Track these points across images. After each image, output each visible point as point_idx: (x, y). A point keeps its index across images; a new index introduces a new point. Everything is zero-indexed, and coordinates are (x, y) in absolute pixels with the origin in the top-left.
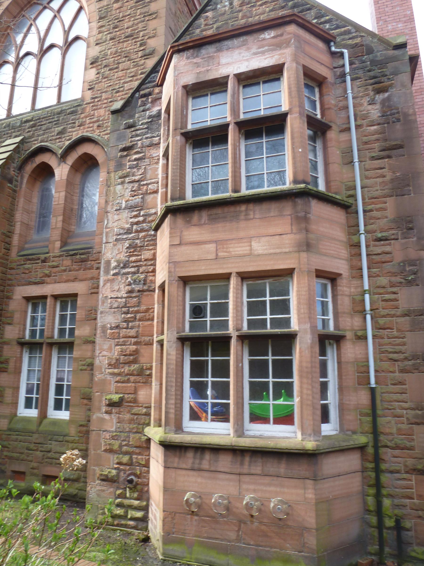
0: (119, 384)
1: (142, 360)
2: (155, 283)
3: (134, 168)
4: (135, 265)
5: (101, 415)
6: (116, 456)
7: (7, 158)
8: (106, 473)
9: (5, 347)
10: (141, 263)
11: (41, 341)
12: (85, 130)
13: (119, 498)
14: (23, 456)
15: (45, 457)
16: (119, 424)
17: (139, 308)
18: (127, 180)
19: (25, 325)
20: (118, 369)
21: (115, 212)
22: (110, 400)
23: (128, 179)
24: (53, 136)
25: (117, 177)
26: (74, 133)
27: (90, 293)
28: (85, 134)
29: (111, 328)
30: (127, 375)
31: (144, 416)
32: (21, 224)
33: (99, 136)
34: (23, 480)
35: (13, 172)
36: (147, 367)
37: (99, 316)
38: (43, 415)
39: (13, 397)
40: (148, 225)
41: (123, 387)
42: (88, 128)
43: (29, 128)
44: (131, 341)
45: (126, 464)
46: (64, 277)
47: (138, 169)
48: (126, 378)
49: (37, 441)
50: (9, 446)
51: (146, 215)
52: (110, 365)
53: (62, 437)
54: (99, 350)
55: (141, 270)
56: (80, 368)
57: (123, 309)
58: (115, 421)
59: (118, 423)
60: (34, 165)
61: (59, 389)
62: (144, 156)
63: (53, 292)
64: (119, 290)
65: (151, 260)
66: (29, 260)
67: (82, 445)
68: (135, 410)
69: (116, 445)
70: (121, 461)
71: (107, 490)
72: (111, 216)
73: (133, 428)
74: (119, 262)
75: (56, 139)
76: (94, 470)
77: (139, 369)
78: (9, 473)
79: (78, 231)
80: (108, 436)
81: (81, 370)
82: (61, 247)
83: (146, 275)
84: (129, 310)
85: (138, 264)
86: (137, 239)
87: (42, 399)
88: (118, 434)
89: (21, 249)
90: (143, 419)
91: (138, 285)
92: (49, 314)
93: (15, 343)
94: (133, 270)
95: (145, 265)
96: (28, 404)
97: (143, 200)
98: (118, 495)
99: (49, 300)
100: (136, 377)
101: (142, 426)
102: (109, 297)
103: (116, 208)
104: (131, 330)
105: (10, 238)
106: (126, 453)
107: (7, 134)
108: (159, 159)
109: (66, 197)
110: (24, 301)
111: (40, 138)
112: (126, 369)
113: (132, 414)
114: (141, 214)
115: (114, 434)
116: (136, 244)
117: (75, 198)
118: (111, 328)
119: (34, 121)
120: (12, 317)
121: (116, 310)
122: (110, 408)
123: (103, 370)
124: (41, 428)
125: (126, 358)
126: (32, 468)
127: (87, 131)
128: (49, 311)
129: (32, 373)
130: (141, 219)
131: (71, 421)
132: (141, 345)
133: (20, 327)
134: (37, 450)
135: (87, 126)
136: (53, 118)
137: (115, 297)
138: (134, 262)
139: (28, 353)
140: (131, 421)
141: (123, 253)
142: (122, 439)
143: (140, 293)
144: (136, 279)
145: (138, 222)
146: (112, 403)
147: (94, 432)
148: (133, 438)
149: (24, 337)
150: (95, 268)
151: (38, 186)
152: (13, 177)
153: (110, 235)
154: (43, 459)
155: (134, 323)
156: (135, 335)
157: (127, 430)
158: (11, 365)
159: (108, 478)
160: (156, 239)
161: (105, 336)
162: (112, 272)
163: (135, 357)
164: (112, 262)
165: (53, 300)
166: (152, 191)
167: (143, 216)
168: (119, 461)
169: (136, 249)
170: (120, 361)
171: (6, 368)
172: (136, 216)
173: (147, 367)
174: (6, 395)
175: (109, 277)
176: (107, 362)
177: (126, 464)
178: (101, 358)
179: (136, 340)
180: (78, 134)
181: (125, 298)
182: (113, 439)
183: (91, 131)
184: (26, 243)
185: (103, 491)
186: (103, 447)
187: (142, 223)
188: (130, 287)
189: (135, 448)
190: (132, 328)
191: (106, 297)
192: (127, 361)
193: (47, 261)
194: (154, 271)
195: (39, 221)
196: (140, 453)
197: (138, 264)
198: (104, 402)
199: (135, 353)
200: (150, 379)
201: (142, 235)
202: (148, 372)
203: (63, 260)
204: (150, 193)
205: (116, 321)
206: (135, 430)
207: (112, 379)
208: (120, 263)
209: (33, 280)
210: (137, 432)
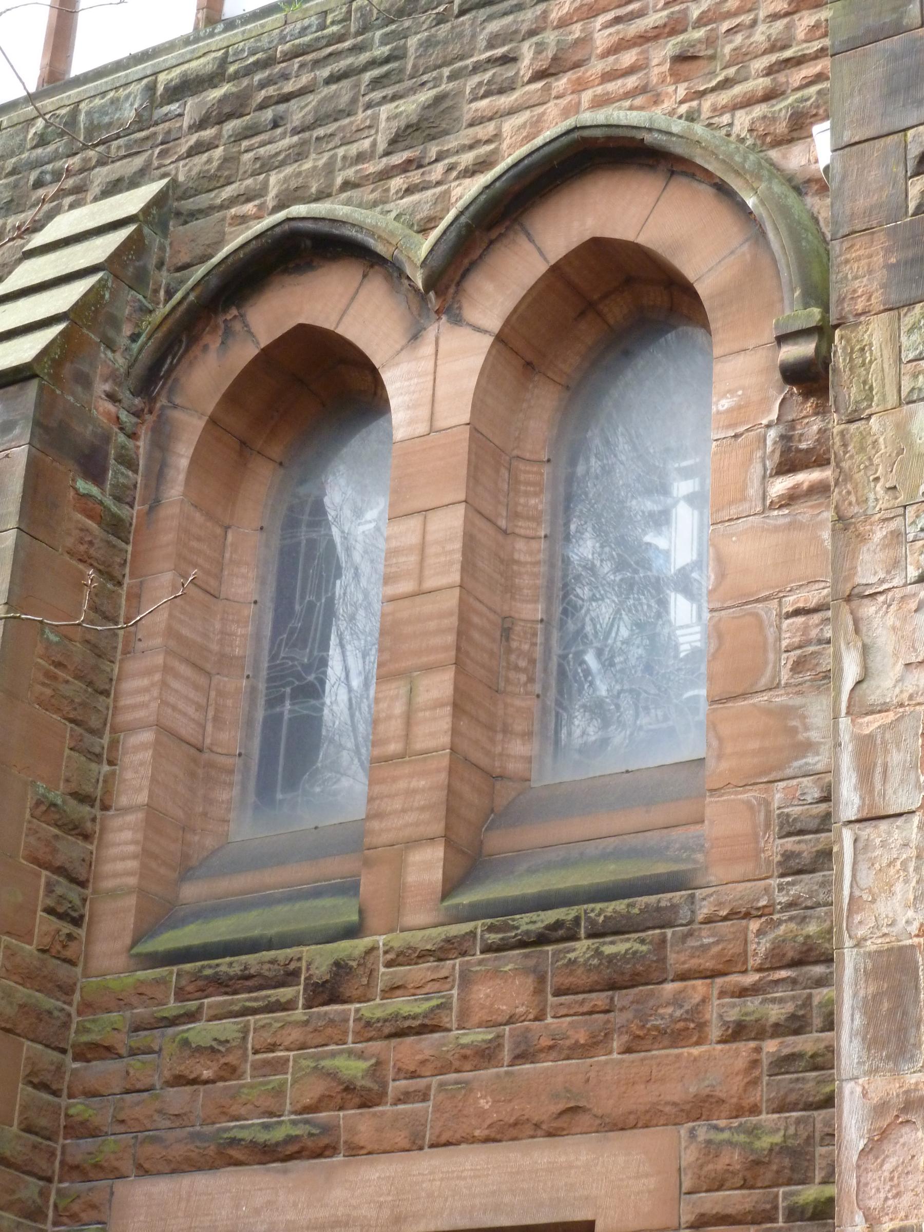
12: (586, 97)
24: (361, 158)
26: (508, 126)
27: (687, 1217)
28: (587, 117)
33: (691, 117)
35: (110, 407)
42: (608, 76)
43: (201, 125)
46: (485, 1104)
66: (222, 984)
72: (891, 620)
75: (386, 175)
82: (450, 888)
107: (57, 176)
109: (470, 543)
117: (521, 550)
119: (236, 76)
127: (599, 103)
135: (597, 67)
136: (357, 49)
150: (715, 1032)
152: (107, 438)
153: (896, 758)
180: (537, 125)
183: (628, 95)
193: (349, 989)
195: (272, 724)
203: (466, 980)
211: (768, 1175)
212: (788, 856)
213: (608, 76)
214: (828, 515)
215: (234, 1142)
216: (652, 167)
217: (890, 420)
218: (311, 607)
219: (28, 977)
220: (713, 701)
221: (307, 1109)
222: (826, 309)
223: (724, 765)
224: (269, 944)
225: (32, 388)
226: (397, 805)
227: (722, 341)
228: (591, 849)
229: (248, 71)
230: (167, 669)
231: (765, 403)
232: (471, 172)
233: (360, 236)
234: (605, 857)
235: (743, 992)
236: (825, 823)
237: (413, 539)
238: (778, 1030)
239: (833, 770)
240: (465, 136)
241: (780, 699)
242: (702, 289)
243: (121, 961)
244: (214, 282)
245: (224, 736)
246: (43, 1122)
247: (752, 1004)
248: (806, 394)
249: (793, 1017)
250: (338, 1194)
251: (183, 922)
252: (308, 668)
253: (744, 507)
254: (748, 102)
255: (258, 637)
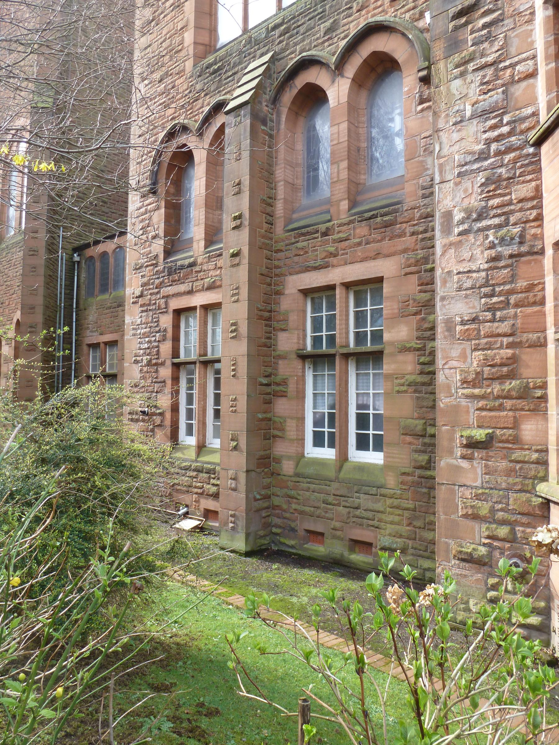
0: (484, 413)
1: (526, 372)
2: (542, 238)
3: (482, 42)
4: (499, 211)
5: (454, 462)
6: (484, 526)
7: (257, 87)
8: (469, 551)
9: (280, 362)
10: (512, 207)
11: (332, 351)
12: (370, 15)
13: (493, 590)
14: (318, 512)
15: (351, 515)
16: (487, 476)
17: (513, 285)
18: (471, 66)
19: (304, 330)
20: (479, 388)
21: (454, 128)
22: (469, 438)
23: (472, 64)
24: (318, 39)
25: (450, 66)
26: (352, 25)
27: (403, 273)
28: (370, 20)
29: (463, 323)
30: (499, 397)
31: (535, 466)
32: (285, 185)
33: (395, 16)
34: (322, 543)
35: (266, 108)
36: (535, 383)
37: (438, 304)
38: (343, 457)
39: (297, 430)
40: (521, 137)
41: (490, 417)
42: (375, 9)
43: (280, 36)
44: (502, 342)
45: (503, 540)
46: (360, 254)
47: (492, 43)
48: (497, 404)
49: (338, 493)
50: (299, 497)
51: (514, 121)
52: (464, 382)
53: (374, 489)
54: (443, 358)
55: (512, 219)
56: (397, 388)
57: (482, 289)
58: (479, 471)
59: (486, 474)
60: (295, 91)
61: (362, 421)
62: (501, 14)
63: (343, 279)
64: (472, 259)
65: (532, 199)
66: (303, 235)
67: (407, 501)
68: (517, 455)
69: (484, 509)
70: (495, 533)
71: (472, 576)
72: (446, 135)
73: (515, 484)
74: (468, 211)
75: (324, 42)
76: (447, 544)
77: (520, 388)
78: (302, 533)
79: (374, 180)
80: (468, 493)
81: (398, 392)
82: (350, 209)
83: (523, 227)
84: (494, 290)
85: (506, 209)
86: (501, 166)
87: (340, 433)
88: (487, 491)
89: (289, 221)
90: (533, 470)
91: (508, 245)
92: (340, 311)
93: (294, 356)
94: (496, 221)
95: (521, 210)
96: (318, 440)
97: (507, 95)
98: (492, 586)
99: (338, 291)
100: (515, 401)
101: (531, 481)
102: (455, 272)
103: (454, 120)
104: (500, 323)
105: (272, 206)
106: (503, 522)
107: (249, 54)
108: (533, 14)
109: (349, 130)
110: (301, 296)
111: (298, 47)
112: (496, 388)
113: (511, 461)
114: (505, 122)
115: (480, 491)
116: (500, 176)
117: (361, 131)
118: (463, 323)
119: (287, 22)
120: (286, 320)
121: (468, 292)
122: (469, 451)
123: (453, 391)
124: (342, 475)
125: (494, 370)
126: (333, 529)
127: (373, 16)
128: (340, 307)
129: (319, 398)
130: (505, 129)
131: (386, 467)
132: (522, 347)
133: (298, 334)
134: (339, 505)
135: (372, 6)
136: (314, 11)
137: (465, 270)
138: (497, 207)
139: (311, 370)
140: (509, 473)
141: (474, 195)
142: (494, 500)
143: (514, 260)
144: (505, 236)
145: (499, 136)
146: (473, 443)
147: (443, 487)
148: (515, 500)
149: (305, 348)
150: (408, 234)
151: (301, 122)
152: (266, 116)
153: (448, 168)
154: (349, 517)
155: (505, 312)
156: (509, 331)
157: (504, 485)
158: (292, 387)
159: (472, 557)
160: (540, 160)
161: (453, 336)
162: (456, 231)
163: (511, 368)
164: (456, 211)
165: (344, 290)
166: (522, 76)
167: (508, 123)
168: (491, 534)
169: (499, 185)
170: (483, 375)
171: (284, 392)
172: (493, 128)
173: (535, 383)
174: (288, 428)
175: (451, 239)
176: (458, 378)
177: (503, 540)
178: (447, 371)
179: (511, 339)
180: (358, 24)
181: (483, 270)
182: (477, 499)
183: (380, 13)
184: (294, 212)
185: (465, 576)
186: (460, 511)
187: (508, 137)
188: (493, 251)
189: (519, 516)
190: (502, 320)
191: (449, 272)
192: (495, 376)
193: (330, 233)
194: (539, 218)
195: (308, 177)
196: (529, 523)
197: (506, 209)
198: (458, 441)
199: (510, 361)
200: (543, 405)
201: (507, 158)
202: (539, 393)
203: (354, 228)
204: (520, 80)
205: (471, 311)
206: (519, 487)
207: (469, 404)
208: (472, 212)
209: (312, 263)
210: (521, 491)
211: (420, 263)
212: (423, 194)
213: (375, 9)
214: (431, 114)
215: (309, 267)
216: (386, 31)
217: (445, 86)
218: (315, 150)
219: (263, 237)
220: (406, 161)
221: (323, 259)
222: (429, 62)
223: (409, 175)
224: (312, 225)
225: (249, 106)
226: (337, 192)
227: (405, 72)
228: (380, 198)
229: (289, 21)
230: (285, 168)
231: (415, 88)
232: (343, 39)
233: (319, 59)
234: (383, 199)
235: (414, 225)
236: (432, 186)
237: (336, 131)
238: (422, 233)
239: (434, 173)
240: (341, 30)
241: (421, 159)
242: (399, 61)
243: (282, 232)
244: (287, 75)
245: (298, 182)
246: (269, 266)
247: (416, 227)
248: (425, 84)
249: (425, 229)
250: (331, 275)
251: (294, 223)
252: (315, 164)
253: (411, 114)
254: (409, 11)
255: (304, 158)
